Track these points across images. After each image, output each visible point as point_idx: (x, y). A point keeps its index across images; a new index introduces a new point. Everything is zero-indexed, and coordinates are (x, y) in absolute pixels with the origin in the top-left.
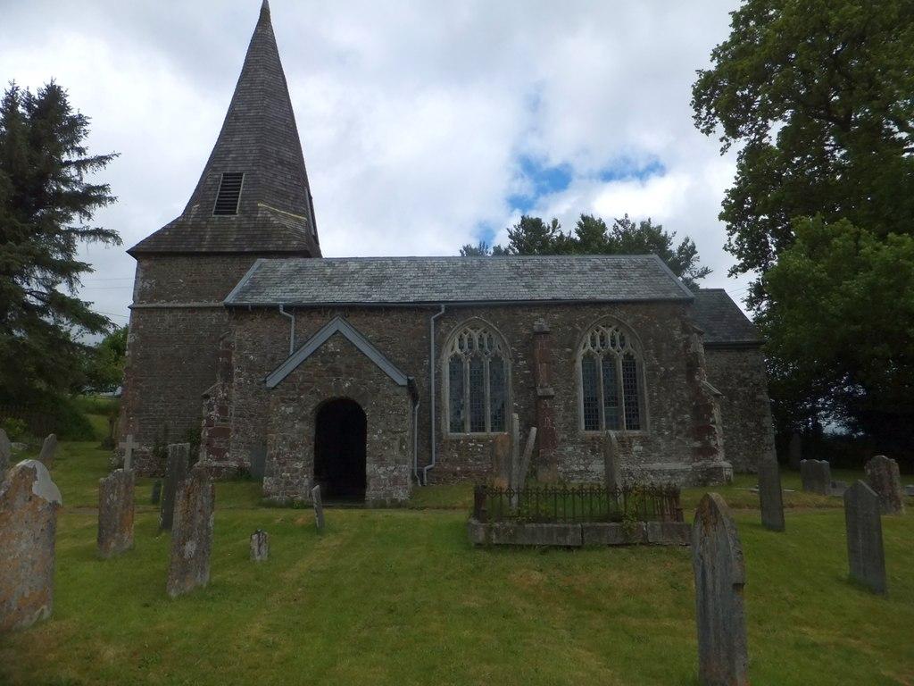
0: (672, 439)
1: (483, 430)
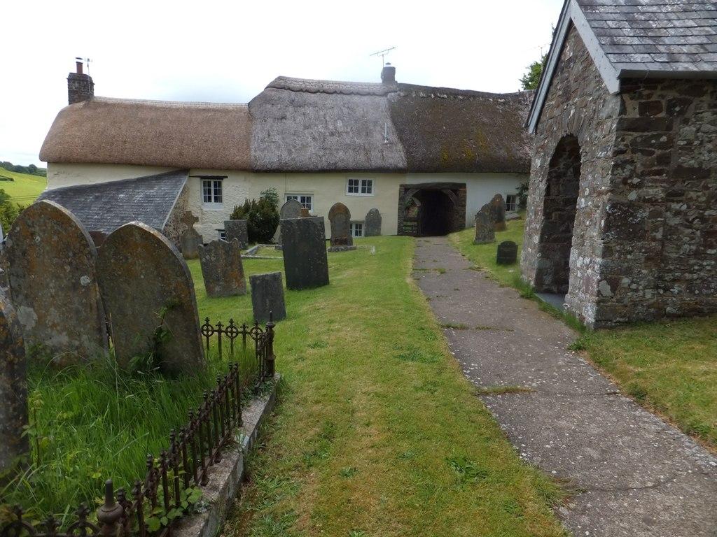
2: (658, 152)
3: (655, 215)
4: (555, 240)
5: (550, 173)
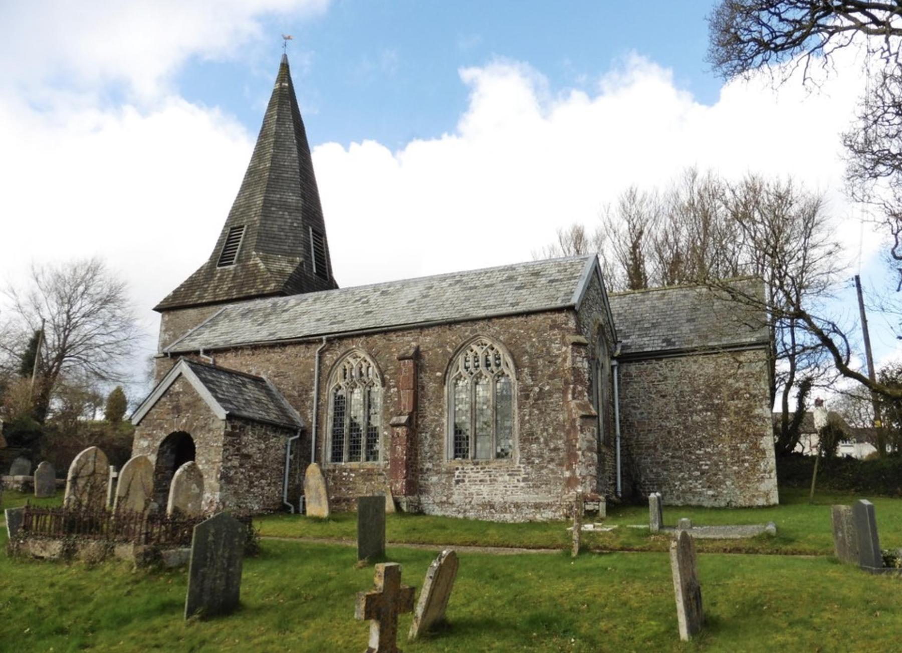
0: (542, 468)
1: (358, 459)
2: (237, 446)
3: (236, 473)
4: (160, 491)
5: (159, 451)
